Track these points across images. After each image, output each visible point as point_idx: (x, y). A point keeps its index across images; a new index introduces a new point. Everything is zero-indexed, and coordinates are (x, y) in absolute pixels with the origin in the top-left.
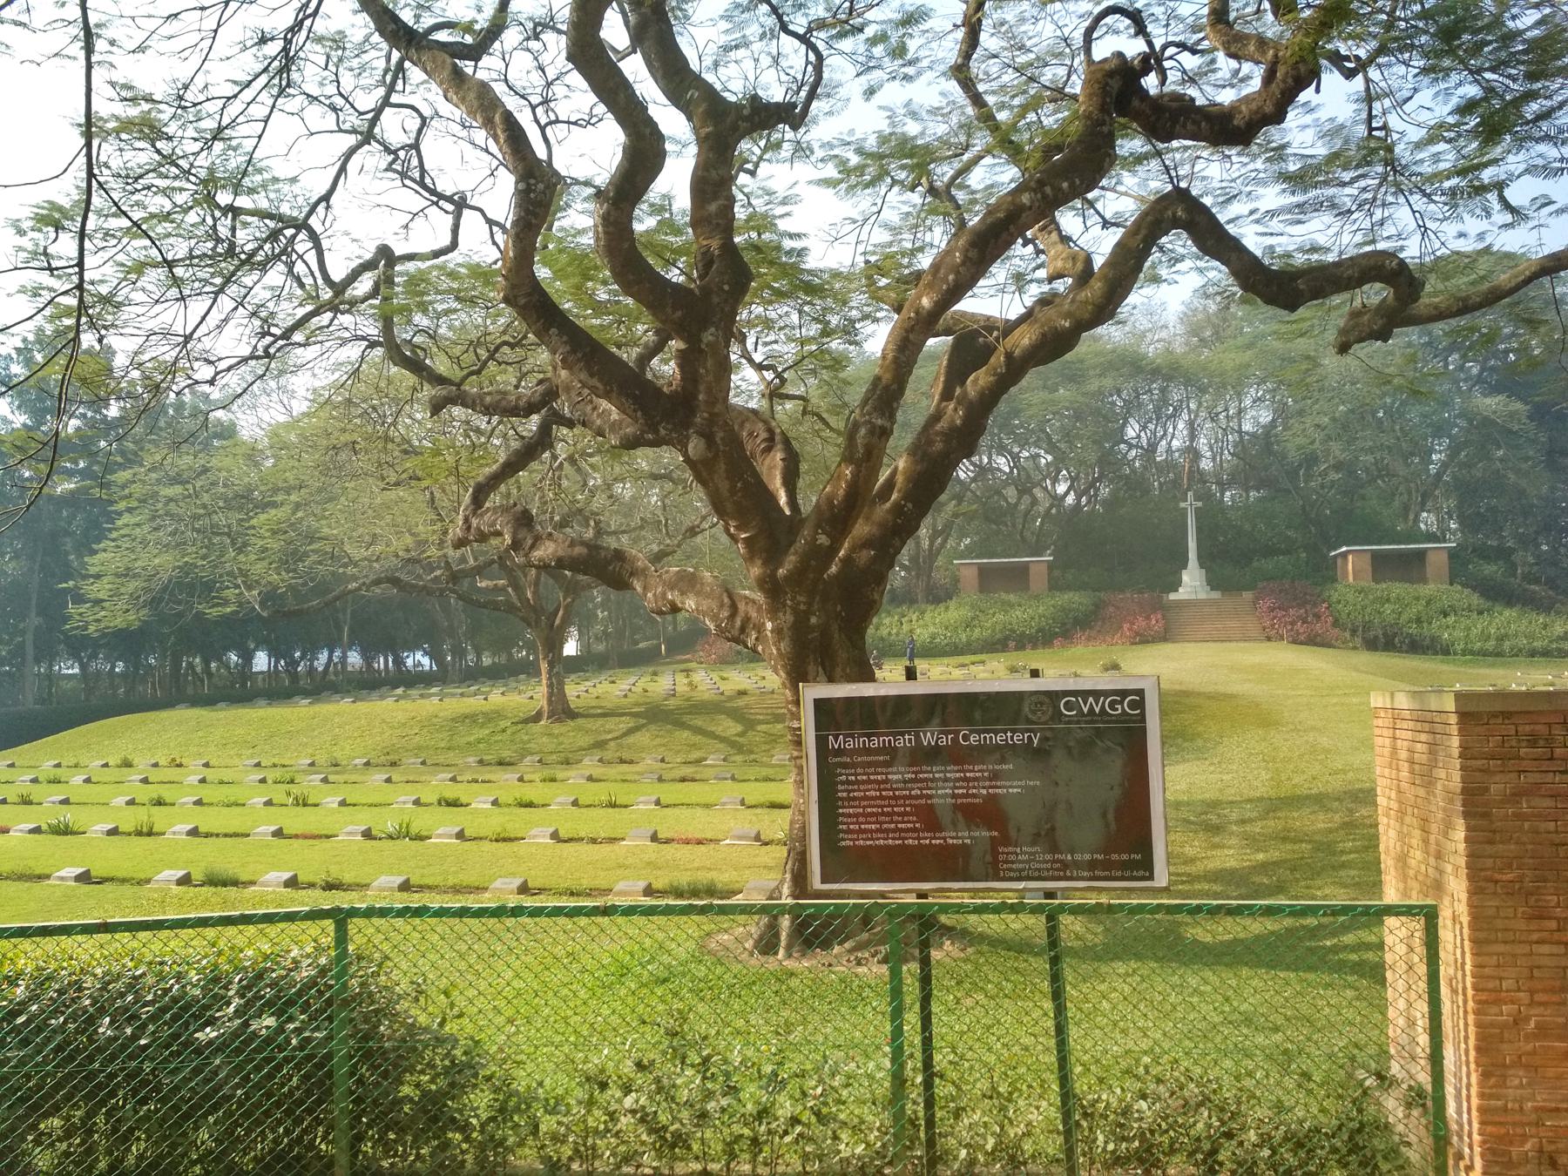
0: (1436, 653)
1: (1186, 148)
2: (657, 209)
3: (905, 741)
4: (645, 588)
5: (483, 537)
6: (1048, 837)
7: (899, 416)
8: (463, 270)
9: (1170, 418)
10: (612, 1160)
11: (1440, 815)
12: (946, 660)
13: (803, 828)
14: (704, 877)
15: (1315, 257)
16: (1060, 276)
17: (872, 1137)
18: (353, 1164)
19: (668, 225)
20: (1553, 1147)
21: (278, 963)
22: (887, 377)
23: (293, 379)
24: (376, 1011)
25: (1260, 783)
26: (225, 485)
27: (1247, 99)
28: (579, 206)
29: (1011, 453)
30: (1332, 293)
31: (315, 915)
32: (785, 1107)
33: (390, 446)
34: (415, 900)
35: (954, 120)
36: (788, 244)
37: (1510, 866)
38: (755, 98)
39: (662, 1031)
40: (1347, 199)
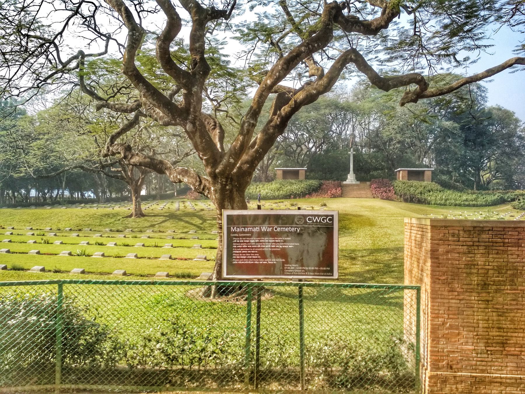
0: (426, 204)
1: (356, 35)
2: (178, 44)
3: (256, 229)
4: (170, 174)
5: (113, 154)
6: (301, 262)
7: (259, 119)
8: (109, 61)
9: (346, 124)
10: (151, 365)
11: (423, 258)
12: (271, 201)
13: (221, 256)
14: (186, 271)
15: (395, 74)
16: (313, 75)
17: (238, 358)
18: (62, 366)
19: (182, 50)
20: (451, 363)
21: (38, 298)
22: (255, 107)
23: (47, 95)
24: (72, 315)
25: (368, 244)
26: (22, 132)
27: (376, 20)
28: (150, 41)
29: (295, 133)
30: (400, 86)
31: (51, 283)
32: (211, 347)
33: (81, 120)
34: (88, 278)
35: (280, 19)
36: (223, 58)
37: (444, 275)
38: (213, 8)
39: (170, 323)
40: (406, 55)
